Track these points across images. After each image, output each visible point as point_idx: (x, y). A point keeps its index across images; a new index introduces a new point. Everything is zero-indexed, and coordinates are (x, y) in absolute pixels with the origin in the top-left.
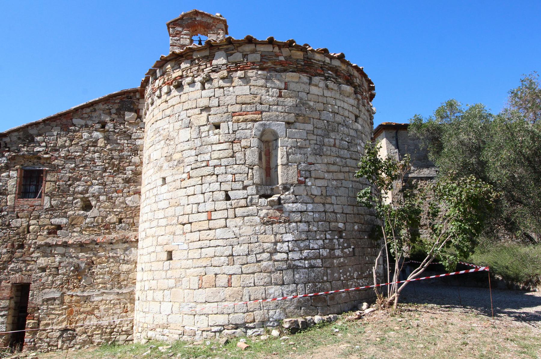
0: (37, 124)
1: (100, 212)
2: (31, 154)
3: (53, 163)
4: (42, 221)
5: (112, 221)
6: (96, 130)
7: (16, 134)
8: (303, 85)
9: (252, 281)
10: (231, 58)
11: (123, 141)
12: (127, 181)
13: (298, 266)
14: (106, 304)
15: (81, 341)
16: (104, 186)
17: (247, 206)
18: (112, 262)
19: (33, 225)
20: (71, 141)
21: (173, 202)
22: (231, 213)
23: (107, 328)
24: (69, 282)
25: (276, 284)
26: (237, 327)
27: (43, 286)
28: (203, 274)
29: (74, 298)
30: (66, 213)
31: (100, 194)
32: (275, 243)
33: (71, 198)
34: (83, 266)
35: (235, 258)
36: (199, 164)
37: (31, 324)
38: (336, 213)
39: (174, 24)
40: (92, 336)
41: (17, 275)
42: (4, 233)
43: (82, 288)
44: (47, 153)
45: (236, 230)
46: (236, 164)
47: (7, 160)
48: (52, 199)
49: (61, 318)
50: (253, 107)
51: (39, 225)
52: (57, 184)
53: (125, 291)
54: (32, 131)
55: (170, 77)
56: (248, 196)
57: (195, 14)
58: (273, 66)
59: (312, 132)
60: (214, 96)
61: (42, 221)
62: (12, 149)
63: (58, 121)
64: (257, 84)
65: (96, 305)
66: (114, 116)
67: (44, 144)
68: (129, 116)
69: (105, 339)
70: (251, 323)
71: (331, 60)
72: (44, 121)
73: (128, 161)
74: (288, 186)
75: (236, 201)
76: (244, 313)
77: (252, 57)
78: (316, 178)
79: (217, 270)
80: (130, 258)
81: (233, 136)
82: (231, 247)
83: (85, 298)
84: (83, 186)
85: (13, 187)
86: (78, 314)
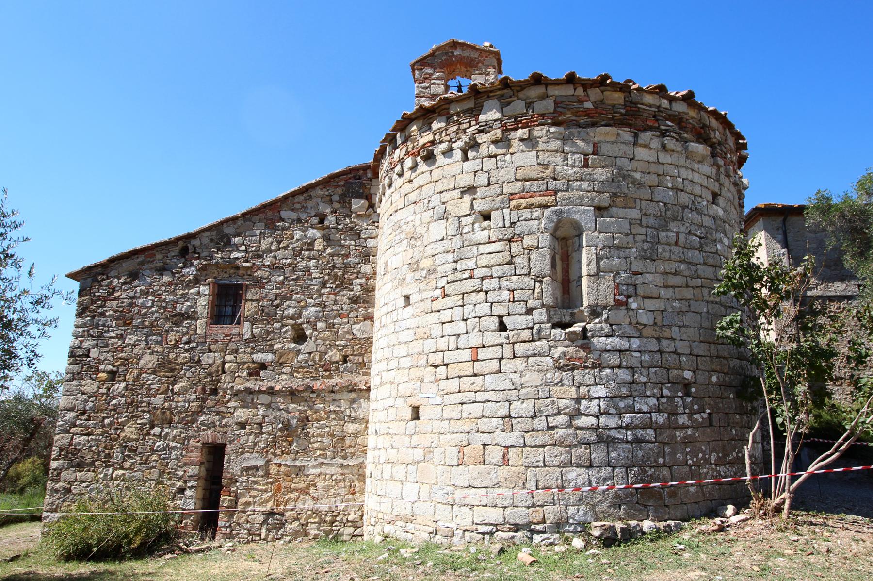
0: (234, 219)
2: (227, 262)
4: (243, 357)
5: (334, 359)
6: (312, 227)
7: (208, 234)
8: (623, 147)
10: (508, 110)
12: (354, 300)
13: (614, 438)
14: (325, 480)
15: (292, 531)
16: (323, 308)
17: (533, 341)
19: (230, 362)
20: (279, 242)
21: (420, 332)
22: (507, 350)
23: (326, 515)
24: (275, 445)
25: (579, 466)
26: (517, 528)
29: (283, 469)
30: (272, 345)
31: (318, 319)
32: (578, 400)
34: (294, 422)
35: (514, 421)
36: (458, 275)
37: (227, 501)
38: (679, 355)
39: (422, 63)
40: (307, 525)
41: (209, 432)
42: (193, 373)
43: (293, 455)
44: (247, 261)
45: (516, 378)
46: (515, 275)
47: (197, 271)
48: (254, 326)
49: (265, 496)
53: (351, 462)
54: (229, 230)
56: (534, 324)
58: (574, 118)
59: (639, 222)
60: (482, 170)
62: (202, 255)
63: (261, 214)
64: (549, 148)
66: (336, 205)
67: (243, 248)
68: (358, 204)
69: (325, 531)
70: (538, 523)
71: (671, 104)
72: (244, 215)
73: (355, 271)
74: (599, 309)
75: (515, 331)
76: (528, 508)
77: (541, 107)
78: (644, 297)
79: (486, 438)
80: (359, 415)
81: (510, 230)
82: (507, 404)
84: (294, 307)
85: (205, 308)
86: (288, 492)
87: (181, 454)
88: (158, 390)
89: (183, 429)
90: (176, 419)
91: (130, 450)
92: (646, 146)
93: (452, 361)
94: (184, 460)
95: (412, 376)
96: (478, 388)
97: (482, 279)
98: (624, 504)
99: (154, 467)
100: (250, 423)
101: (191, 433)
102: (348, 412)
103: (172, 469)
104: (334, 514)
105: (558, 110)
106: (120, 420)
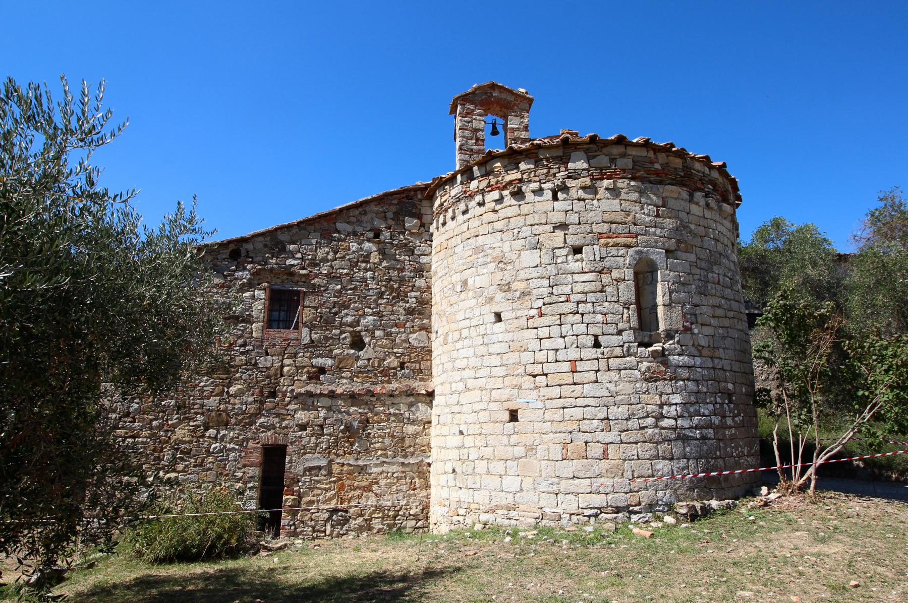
0: (289, 227)
1: (376, 352)
2: (282, 268)
3: (313, 282)
4: (300, 361)
5: (392, 365)
6: (369, 240)
7: (261, 239)
8: (682, 202)
9: (635, 452)
10: (594, 162)
11: (403, 257)
12: (410, 312)
13: (688, 436)
14: (387, 478)
15: (356, 526)
16: (380, 317)
17: (624, 357)
18: (394, 421)
19: (288, 366)
20: (336, 253)
21: (516, 345)
22: (603, 364)
23: (389, 510)
24: (337, 446)
25: (664, 458)
26: (618, 510)
27: (304, 451)
28: (568, 441)
29: (346, 468)
30: (331, 351)
31: (376, 328)
32: (661, 406)
33: (338, 331)
34: (356, 424)
35: (612, 423)
36: (554, 298)
37: (290, 500)
38: (725, 371)
39: (465, 99)
40: (371, 520)
41: (269, 434)
42: (250, 375)
43: (356, 455)
44: (303, 269)
45: (612, 387)
46: (607, 301)
47: (251, 274)
48: (313, 332)
49: (328, 494)
50: (626, 228)
51: (296, 367)
52: (319, 311)
53: (412, 461)
54: (283, 237)
55: (500, 179)
56: (624, 343)
57: (490, 88)
58: (646, 175)
60: (572, 210)
61: (300, 361)
62: (256, 259)
63: (316, 224)
64: (630, 198)
65: (376, 479)
66: (391, 222)
67: (299, 255)
68: (411, 223)
69: (388, 525)
70: (635, 506)
71: (710, 171)
72: (299, 223)
73: (410, 284)
75: (609, 349)
76: (626, 493)
77: (621, 163)
78: (702, 325)
79: (587, 437)
80: (417, 417)
81: (600, 264)
82: (605, 408)
83: (360, 469)
84: (352, 316)
85: (261, 312)
86: (351, 490)
87: (240, 456)
88: (212, 392)
89: (241, 431)
90: (233, 421)
91: (182, 452)
92: (697, 204)
93: (552, 372)
94: (243, 462)
95: (506, 384)
96: (578, 395)
97: (578, 303)
98: (697, 488)
99: (210, 469)
100: (312, 425)
101: (249, 435)
102: (407, 415)
103: (230, 470)
104: (396, 509)
105: (636, 167)
106: (170, 422)
